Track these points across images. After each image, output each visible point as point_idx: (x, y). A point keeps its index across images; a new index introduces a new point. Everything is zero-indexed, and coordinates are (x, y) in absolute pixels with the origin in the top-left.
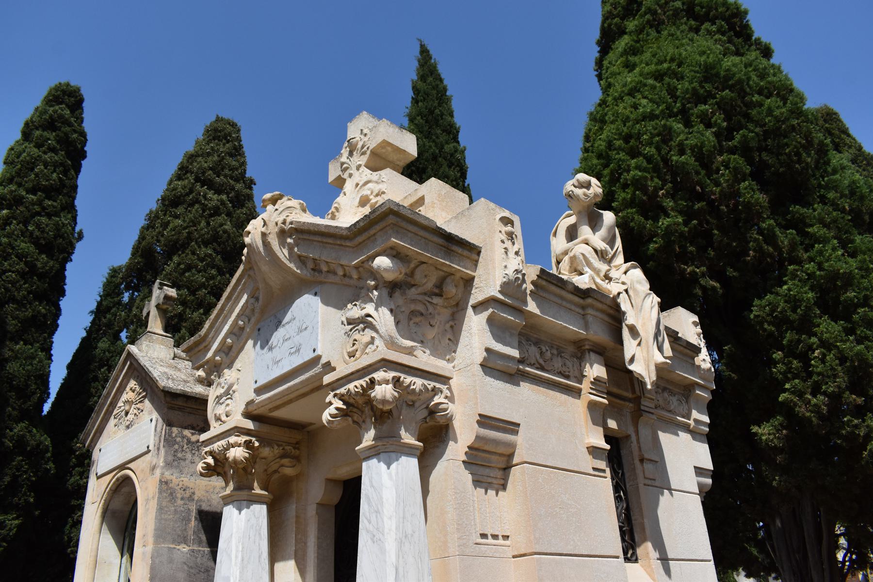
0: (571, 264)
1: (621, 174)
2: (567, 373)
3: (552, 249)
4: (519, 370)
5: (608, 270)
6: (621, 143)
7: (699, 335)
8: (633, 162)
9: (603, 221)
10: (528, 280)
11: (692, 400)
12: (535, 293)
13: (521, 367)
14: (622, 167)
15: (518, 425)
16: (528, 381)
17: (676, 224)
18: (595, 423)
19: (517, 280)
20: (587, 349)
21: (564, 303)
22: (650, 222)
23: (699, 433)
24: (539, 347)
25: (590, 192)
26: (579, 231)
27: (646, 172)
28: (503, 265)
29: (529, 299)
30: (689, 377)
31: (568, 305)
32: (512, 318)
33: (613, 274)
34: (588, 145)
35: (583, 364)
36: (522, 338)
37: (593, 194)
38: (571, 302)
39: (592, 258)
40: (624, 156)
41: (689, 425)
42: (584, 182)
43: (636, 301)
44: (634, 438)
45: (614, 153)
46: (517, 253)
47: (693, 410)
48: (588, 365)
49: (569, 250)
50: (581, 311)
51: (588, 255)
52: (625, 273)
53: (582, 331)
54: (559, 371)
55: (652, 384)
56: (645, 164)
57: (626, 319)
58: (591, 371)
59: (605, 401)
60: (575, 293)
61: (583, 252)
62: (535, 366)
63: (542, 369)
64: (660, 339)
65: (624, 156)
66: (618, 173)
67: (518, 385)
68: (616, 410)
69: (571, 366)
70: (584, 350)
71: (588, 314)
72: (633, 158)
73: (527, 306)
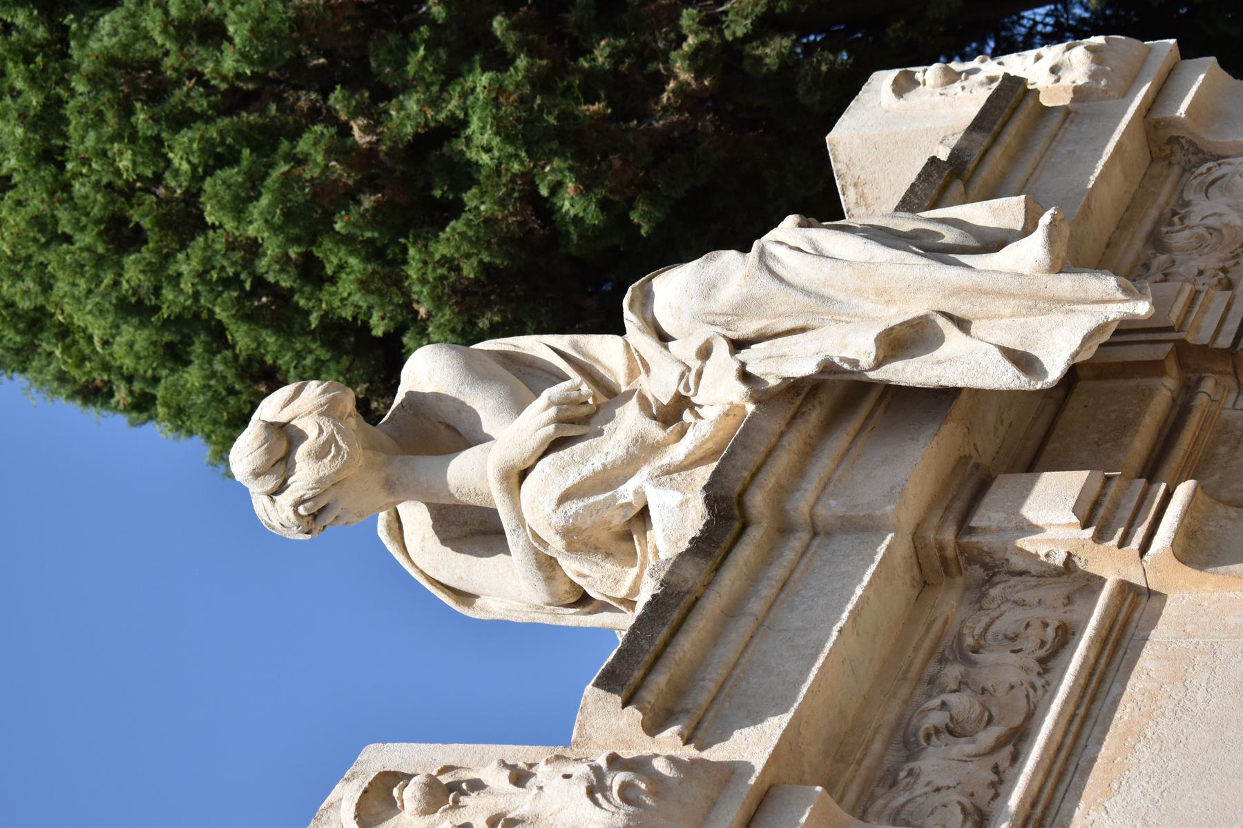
0: (596, 549)
1: (260, 283)
2: (1050, 633)
3: (524, 618)
5: (644, 404)
6: (136, 262)
10: (637, 745)
11: (1210, 138)
12: (699, 723)
14: (230, 271)
21: (756, 606)
22: (470, 198)
26: (464, 499)
29: (717, 753)
30: (1116, 136)
31: (767, 590)
33: (662, 387)
34: (121, 394)
35: (1018, 563)
36: (880, 802)
37: (324, 422)
38: (754, 578)
39: (584, 461)
42: (269, 451)
45: (168, 293)
46: (520, 777)
48: (1026, 543)
49: (537, 553)
50: (797, 542)
52: (663, 338)
53: (881, 550)
54: (1037, 668)
56: (232, 174)
57: (855, 363)
58: (1050, 533)
59: (1184, 491)
60: (719, 553)
61: (557, 493)
62: (1004, 764)
63: (1019, 737)
64: (950, 236)
68: (1222, 450)
69: (1021, 614)
70: (961, 549)
73: (747, 768)
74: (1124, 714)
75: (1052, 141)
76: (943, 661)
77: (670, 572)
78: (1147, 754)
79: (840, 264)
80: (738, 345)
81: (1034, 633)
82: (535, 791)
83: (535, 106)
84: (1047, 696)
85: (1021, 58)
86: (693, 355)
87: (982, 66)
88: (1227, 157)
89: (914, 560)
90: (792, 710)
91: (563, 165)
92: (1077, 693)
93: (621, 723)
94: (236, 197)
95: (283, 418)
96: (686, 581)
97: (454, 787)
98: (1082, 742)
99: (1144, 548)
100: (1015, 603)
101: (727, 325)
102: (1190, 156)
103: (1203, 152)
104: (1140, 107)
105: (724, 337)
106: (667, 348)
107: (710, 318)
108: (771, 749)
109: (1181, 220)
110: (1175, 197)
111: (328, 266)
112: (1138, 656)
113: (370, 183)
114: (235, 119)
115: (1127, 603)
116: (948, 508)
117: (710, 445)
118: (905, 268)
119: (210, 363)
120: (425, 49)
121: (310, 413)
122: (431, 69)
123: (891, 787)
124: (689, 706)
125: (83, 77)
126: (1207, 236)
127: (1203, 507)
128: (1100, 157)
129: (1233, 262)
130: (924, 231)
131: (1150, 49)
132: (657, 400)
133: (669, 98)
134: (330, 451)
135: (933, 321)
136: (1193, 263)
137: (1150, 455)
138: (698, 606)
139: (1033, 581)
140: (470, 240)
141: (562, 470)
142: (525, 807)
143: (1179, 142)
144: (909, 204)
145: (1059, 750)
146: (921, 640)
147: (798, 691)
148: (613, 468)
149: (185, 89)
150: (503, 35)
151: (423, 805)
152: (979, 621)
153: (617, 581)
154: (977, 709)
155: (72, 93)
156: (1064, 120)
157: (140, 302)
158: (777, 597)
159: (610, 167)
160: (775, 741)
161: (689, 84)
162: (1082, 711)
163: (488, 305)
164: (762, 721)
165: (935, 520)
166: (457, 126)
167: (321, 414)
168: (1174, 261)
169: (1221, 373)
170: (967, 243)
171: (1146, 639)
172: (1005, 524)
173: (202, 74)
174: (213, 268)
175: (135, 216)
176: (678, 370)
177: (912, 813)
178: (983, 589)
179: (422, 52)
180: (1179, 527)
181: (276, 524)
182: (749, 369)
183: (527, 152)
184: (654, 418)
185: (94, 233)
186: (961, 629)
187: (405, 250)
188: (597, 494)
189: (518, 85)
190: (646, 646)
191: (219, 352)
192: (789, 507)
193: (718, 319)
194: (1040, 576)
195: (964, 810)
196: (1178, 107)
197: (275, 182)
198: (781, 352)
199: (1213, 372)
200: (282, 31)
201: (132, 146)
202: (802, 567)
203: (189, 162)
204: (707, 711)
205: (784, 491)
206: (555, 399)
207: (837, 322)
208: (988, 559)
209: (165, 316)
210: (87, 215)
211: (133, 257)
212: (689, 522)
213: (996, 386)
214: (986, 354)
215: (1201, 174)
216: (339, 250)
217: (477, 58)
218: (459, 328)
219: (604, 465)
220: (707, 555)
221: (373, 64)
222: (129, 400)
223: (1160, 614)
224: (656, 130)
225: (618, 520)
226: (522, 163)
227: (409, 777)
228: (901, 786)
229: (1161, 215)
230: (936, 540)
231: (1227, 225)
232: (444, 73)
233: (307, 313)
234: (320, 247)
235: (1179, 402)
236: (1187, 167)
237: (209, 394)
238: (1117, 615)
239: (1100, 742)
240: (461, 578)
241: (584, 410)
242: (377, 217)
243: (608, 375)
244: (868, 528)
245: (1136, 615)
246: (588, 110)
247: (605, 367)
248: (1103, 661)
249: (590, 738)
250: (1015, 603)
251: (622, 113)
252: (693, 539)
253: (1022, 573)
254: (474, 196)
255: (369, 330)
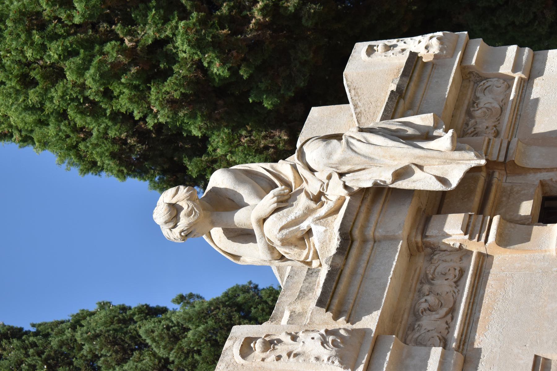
0: (292, 244)
1: (86, 99)
2: (457, 272)
3: (259, 264)
4: (458, 349)
5: (307, 193)
6: (34, 93)
7: (388, 48)
8: (70, 77)
9: (226, 189)
10: (333, 325)
11: (484, 72)
12: (350, 315)
13: (454, 345)
14: (75, 95)
15: (536, 357)
16: (472, 335)
17: (186, 31)
18: (527, 238)
19: (336, 344)
20: (422, 239)
21: (361, 271)
22: (176, 68)
23: (532, 63)
24: (422, 312)
25: (185, 207)
26: (240, 227)
27: (90, 61)
28: (314, 362)
29: (358, 325)
30: (452, 75)
31: (363, 265)
32: (389, 354)
33: (313, 187)
34: (16, 136)
35: (443, 247)
36: (410, 337)
37: (189, 202)
38: (358, 260)
39: (288, 216)
40: (56, 91)
41: (521, 79)
42: (170, 215)
43: (356, 162)
44: (544, 176)
45: (48, 104)
46: (294, 338)
47: (500, 71)
48: (446, 241)
49: (268, 245)
50: (370, 246)
51: (284, 222)
52: (312, 171)
53: (399, 247)
54: (454, 285)
55: (478, 157)
56: (78, 60)
57: (385, 182)
58: (454, 237)
59: (496, 219)
60: (346, 253)
61: (279, 227)
62: (449, 321)
63: (453, 311)
64: (410, 131)
65: (56, 91)
66: (84, 103)
67: (479, 351)
68: (504, 199)
69: (445, 264)
70: (423, 243)
71: (374, 236)
72: (64, 77)
73: (369, 330)
74: (486, 301)
75: (429, 77)
76: (421, 283)
77: (332, 262)
78: (496, 316)
79: (377, 147)
80: (341, 175)
81: (452, 272)
82: (302, 344)
83: (202, 33)
84: (459, 295)
85: (413, 41)
86: (325, 178)
87: (398, 43)
88: (490, 78)
89: (408, 248)
90: (381, 309)
91: (214, 55)
92: (470, 294)
93: (325, 317)
94: (79, 68)
95: (173, 201)
96: (338, 264)
97: (271, 342)
98: (474, 311)
99: (486, 241)
100: (443, 261)
101: (336, 168)
102: (477, 78)
103: (481, 77)
104: (458, 62)
105: (336, 172)
106: (314, 175)
107: (330, 165)
108: (376, 323)
109: (477, 105)
110: (473, 95)
111: (115, 92)
112: (487, 279)
113: (134, 62)
114: (75, 37)
115: (481, 260)
116: (417, 228)
117: (333, 209)
118: (400, 149)
119: (59, 126)
120: (155, 10)
121: (184, 199)
122: (158, 18)
123: (412, 331)
124: (346, 309)
125: (11, 20)
126: (487, 111)
127: (503, 224)
128: (448, 84)
129: (497, 123)
130: (400, 129)
131: (458, 36)
132: (312, 193)
133: (253, 26)
134: (192, 213)
135: (411, 167)
136: (484, 124)
137: (480, 202)
138: (343, 273)
139: (448, 253)
140: (177, 85)
141: (280, 219)
142: (299, 349)
143: (473, 73)
144: (389, 114)
145: (467, 315)
146: (413, 276)
147: (382, 301)
148: (298, 218)
149: (53, 24)
150: (185, 2)
151: (263, 349)
152: (431, 268)
153: (300, 255)
154: (437, 301)
155: (6, 27)
156: (432, 68)
157: (34, 106)
158: (366, 266)
159: (232, 55)
160: (377, 321)
161: (260, 20)
162: (472, 301)
163: (183, 107)
164: (371, 313)
165: (414, 234)
166: (168, 40)
167: (188, 200)
168: (476, 122)
169: (501, 170)
170: (416, 134)
171: (489, 273)
172: (438, 234)
173: (61, 19)
174: (67, 94)
175: (32, 74)
176: (320, 184)
177: (421, 340)
178: (431, 256)
179: (154, 12)
180: (497, 233)
181: (172, 238)
182: (347, 184)
183: (200, 51)
184: (312, 200)
185: (15, 81)
186: (426, 271)
187: (150, 89)
188: (293, 227)
189: (194, 24)
190: (330, 290)
191: (62, 121)
192: (366, 233)
193: (333, 166)
194: (451, 251)
195: (439, 339)
196: (472, 61)
197: (96, 63)
198: (358, 178)
199: (498, 169)
200: (97, 5)
201: (32, 47)
202: (373, 254)
203: (57, 54)
204: (352, 310)
205: (364, 228)
206: (276, 194)
207: (376, 166)
208: (433, 246)
209: (47, 113)
210: (11, 73)
211: (32, 91)
212: (327, 236)
213: (434, 190)
214: (430, 179)
215: (481, 85)
216: (120, 87)
217: (176, 12)
218: (171, 116)
219: (295, 217)
220: (343, 254)
221: (133, 16)
222: (20, 139)
223: (492, 263)
224: (247, 38)
225: (299, 235)
226: (198, 56)
227: (256, 339)
228: (416, 330)
229: (469, 103)
230: (415, 241)
231: (494, 107)
232: (163, 19)
233: (105, 110)
234: (111, 85)
235: (487, 180)
236: (476, 81)
237: (58, 138)
238: (478, 264)
239: (480, 311)
240: (236, 251)
241: (286, 197)
242: (137, 76)
243: (285, 178)
244: (394, 239)
245: (485, 263)
246: (222, 32)
247: (284, 175)
248: (476, 282)
249: (314, 322)
250: (443, 261)
251: (234, 33)
252: (337, 248)
253: (444, 251)
254: (177, 67)
255: (134, 117)
